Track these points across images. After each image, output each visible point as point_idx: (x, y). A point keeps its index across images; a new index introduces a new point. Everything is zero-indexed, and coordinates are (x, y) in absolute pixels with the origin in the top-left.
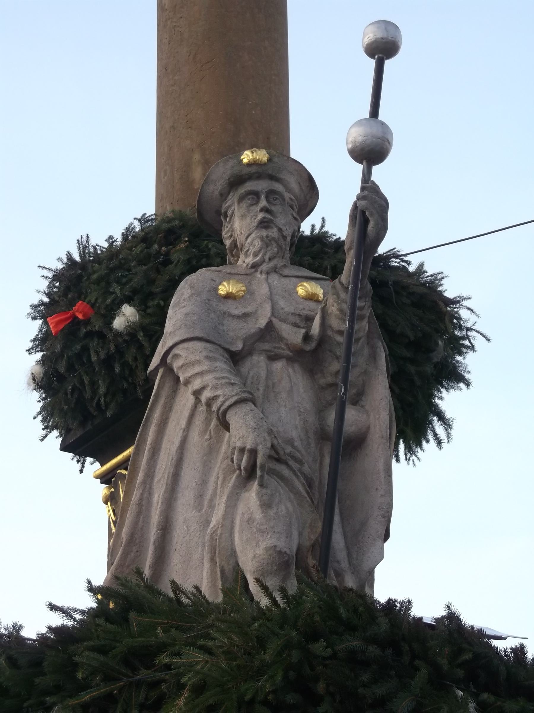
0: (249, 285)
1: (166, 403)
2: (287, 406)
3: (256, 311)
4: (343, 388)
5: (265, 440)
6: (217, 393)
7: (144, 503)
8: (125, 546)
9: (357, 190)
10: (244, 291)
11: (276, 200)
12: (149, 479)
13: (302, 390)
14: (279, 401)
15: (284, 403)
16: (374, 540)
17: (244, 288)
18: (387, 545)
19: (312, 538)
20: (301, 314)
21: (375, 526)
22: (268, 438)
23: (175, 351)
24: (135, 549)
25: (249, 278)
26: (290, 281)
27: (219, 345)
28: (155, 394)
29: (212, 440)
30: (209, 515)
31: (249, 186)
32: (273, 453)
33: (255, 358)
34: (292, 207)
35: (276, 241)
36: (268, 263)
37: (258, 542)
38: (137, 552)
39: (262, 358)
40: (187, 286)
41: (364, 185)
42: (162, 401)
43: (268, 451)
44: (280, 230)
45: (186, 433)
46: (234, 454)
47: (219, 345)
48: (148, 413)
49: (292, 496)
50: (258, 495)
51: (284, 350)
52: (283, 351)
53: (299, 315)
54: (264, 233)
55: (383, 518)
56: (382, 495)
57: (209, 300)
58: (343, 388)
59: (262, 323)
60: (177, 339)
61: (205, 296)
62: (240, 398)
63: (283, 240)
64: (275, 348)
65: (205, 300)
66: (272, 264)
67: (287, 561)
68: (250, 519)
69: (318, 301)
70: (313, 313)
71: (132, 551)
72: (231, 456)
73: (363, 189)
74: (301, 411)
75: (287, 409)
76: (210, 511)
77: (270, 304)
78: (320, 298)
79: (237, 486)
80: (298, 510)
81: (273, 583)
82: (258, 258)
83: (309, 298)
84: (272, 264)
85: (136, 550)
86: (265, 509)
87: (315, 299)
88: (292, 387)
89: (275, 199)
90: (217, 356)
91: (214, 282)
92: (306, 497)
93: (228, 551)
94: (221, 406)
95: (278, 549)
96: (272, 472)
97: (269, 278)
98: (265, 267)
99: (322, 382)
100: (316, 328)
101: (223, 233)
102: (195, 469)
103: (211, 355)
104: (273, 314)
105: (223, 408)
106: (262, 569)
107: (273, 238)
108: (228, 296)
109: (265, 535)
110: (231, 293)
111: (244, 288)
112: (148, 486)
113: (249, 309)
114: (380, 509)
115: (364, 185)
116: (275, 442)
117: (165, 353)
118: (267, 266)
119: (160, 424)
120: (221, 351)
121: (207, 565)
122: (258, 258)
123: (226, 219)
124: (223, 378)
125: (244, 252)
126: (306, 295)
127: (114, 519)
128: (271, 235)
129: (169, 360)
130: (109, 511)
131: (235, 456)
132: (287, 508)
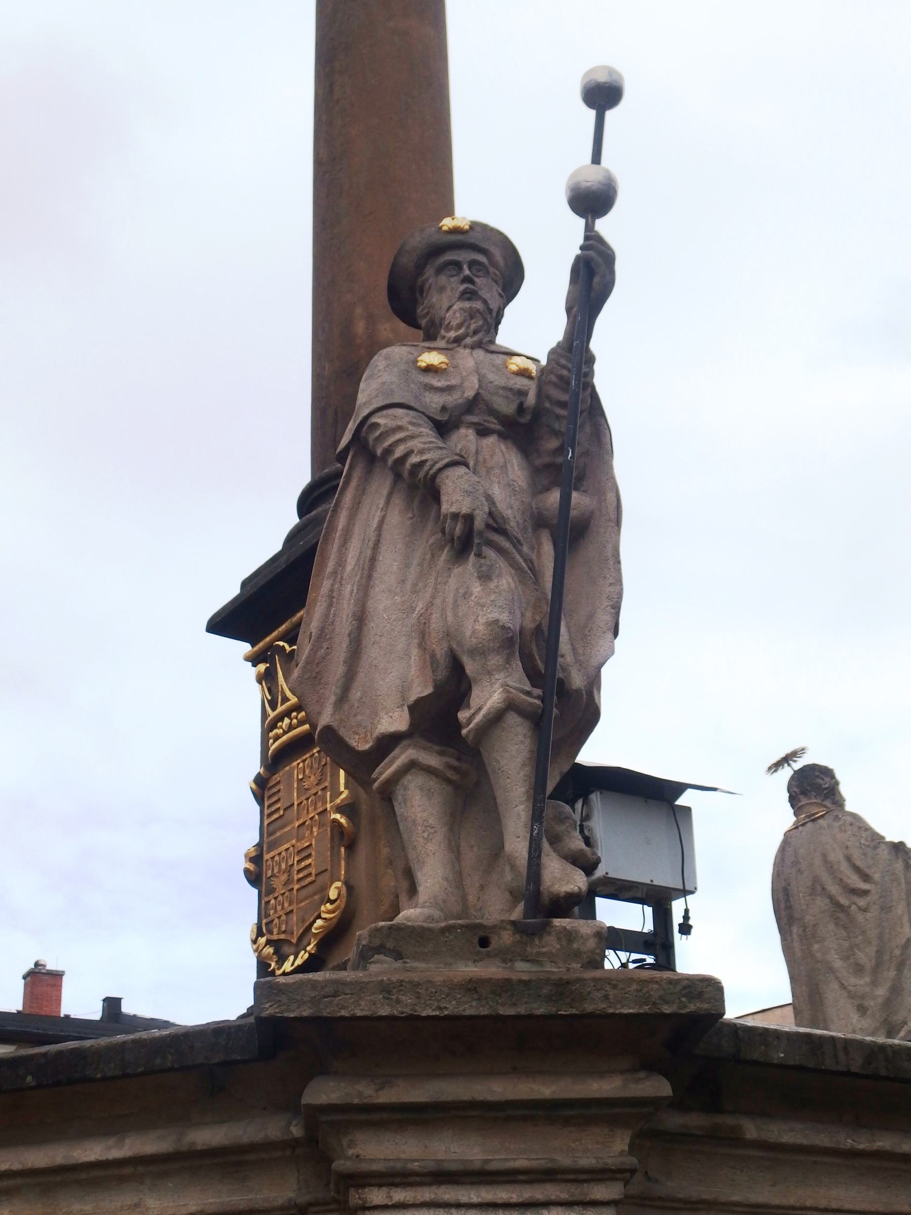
0: (452, 358)
1: (359, 485)
2: (501, 482)
3: (462, 383)
4: (570, 451)
5: (482, 504)
6: (424, 458)
7: (335, 594)
8: (314, 641)
9: (580, 241)
10: (447, 364)
11: (479, 271)
12: (341, 568)
13: (516, 468)
14: (492, 478)
15: (498, 480)
16: (604, 632)
17: (446, 360)
18: (618, 642)
19: (537, 619)
20: (513, 388)
21: (603, 618)
22: (486, 503)
23: (374, 419)
24: (325, 645)
25: (451, 352)
26: (498, 357)
27: (423, 413)
28: (346, 474)
29: (415, 519)
30: (414, 601)
31: (449, 256)
32: (491, 522)
33: (463, 431)
34: (496, 282)
35: (480, 313)
36: (471, 337)
37: (477, 617)
38: (328, 648)
39: (471, 431)
40: (381, 358)
41: (588, 233)
42: (354, 483)
43: (485, 516)
44: (485, 302)
45: (385, 513)
46: (446, 522)
47: (423, 413)
48: (337, 498)
49: (513, 572)
50: (474, 565)
51: (494, 424)
52: (494, 426)
53: (511, 390)
54: (467, 305)
55: (613, 609)
56: (611, 584)
57: (408, 371)
58: (570, 451)
59: (470, 394)
60: (375, 405)
61: (403, 367)
62: (451, 461)
63: (488, 314)
64: (485, 421)
65: (403, 371)
66: (476, 338)
67: (512, 638)
68: (466, 593)
69: (530, 377)
70: (526, 388)
71: (322, 648)
72: (443, 524)
73: (587, 238)
74: (516, 491)
75: (501, 485)
76: (414, 596)
77: (477, 377)
78: (533, 374)
79: (448, 561)
80: (520, 588)
81: (495, 662)
82: (461, 331)
83: (520, 373)
84: (476, 338)
85: (326, 646)
86: (484, 582)
87: (527, 375)
88: (505, 462)
89: (478, 270)
90: (422, 422)
91: (411, 355)
92: (529, 573)
93: (440, 634)
94: (430, 469)
95: (501, 624)
96: (491, 544)
97: (300, 830)
98: (468, 340)
99: (538, 462)
100: (531, 399)
101: (419, 311)
102: (396, 552)
103: (414, 421)
104: (480, 387)
105: (432, 472)
106: (483, 646)
107: (478, 311)
108: (429, 369)
109: (485, 609)
110: (432, 365)
111: (446, 360)
112: (339, 576)
113: (453, 382)
114: (609, 599)
115: (588, 233)
116: (493, 509)
117: (359, 425)
118: (472, 340)
119: (353, 508)
120: (426, 419)
121: (415, 652)
122: (461, 331)
123: (422, 295)
124: (430, 442)
125: (443, 327)
126: (518, 370)
127: (269, 698)
128: (476, 307)
129: (363, 434)
130: (263, 691)
131: (447, 525)
132: (508, 582)
